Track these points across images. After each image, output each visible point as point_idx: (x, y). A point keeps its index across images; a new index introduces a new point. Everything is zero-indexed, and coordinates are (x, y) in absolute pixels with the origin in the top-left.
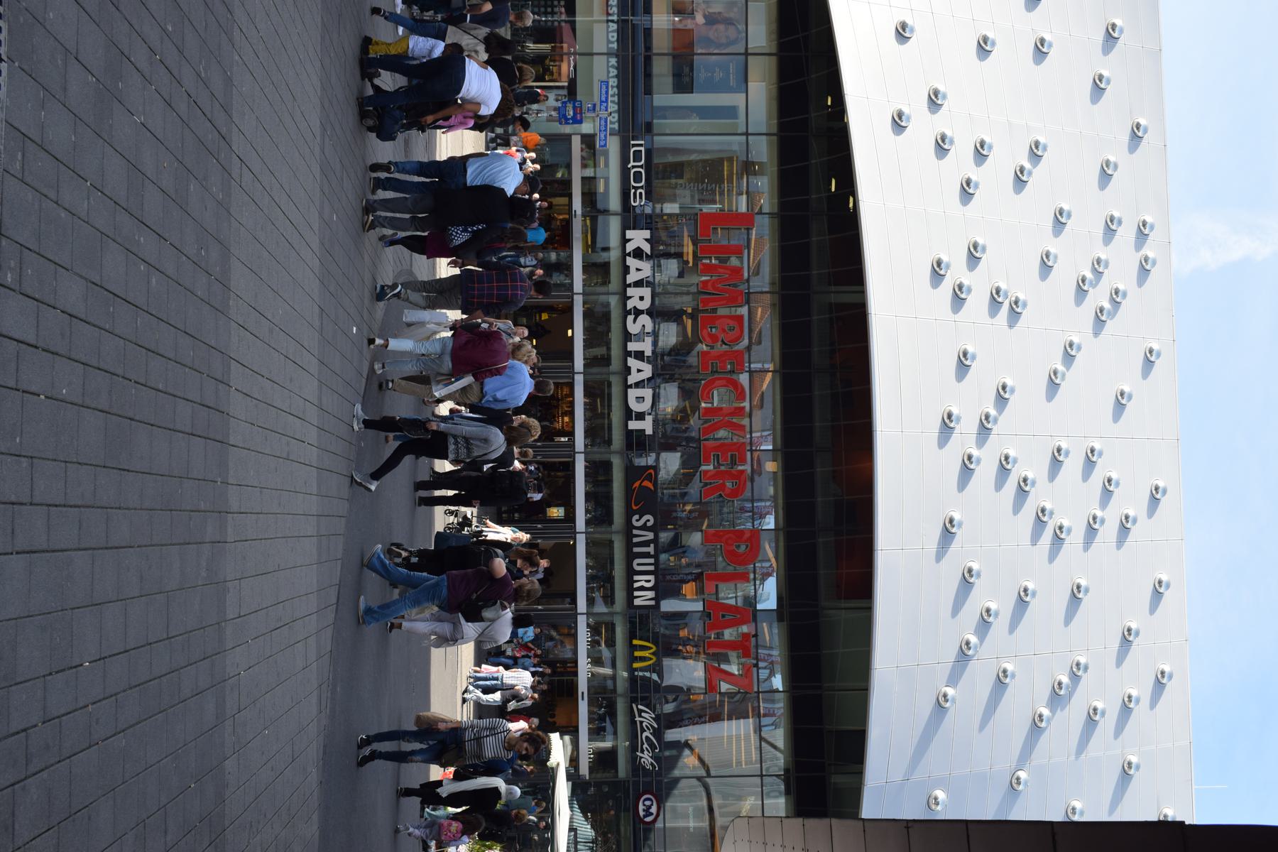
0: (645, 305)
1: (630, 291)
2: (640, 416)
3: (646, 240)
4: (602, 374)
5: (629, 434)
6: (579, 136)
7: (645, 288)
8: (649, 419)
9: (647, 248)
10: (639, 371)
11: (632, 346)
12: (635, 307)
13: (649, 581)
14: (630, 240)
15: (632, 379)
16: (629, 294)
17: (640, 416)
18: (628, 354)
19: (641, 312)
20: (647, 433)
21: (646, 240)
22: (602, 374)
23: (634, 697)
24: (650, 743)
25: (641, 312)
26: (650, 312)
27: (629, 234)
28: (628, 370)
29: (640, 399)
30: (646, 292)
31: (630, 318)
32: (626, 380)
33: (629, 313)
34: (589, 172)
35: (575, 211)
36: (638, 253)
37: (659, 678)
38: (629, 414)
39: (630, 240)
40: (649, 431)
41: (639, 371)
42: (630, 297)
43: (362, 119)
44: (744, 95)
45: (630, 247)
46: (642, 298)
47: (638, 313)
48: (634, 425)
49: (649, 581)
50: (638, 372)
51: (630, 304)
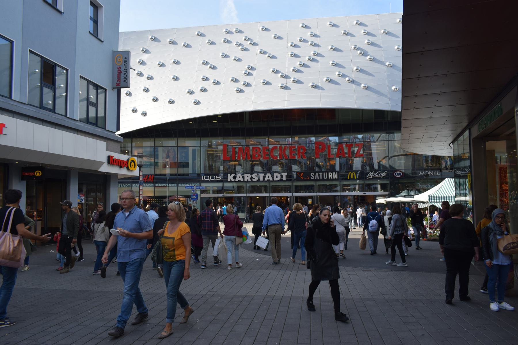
1: (246, 180)
2: (282, 177)
3: (231, 175)
5: (287, 180)
8: (283, 174)
9: (233, 175)
10: (269, 177)
11: (261, 179)
12: (250, 178)
14: (231, 180)
15: (271, 179)
16: (230, 181)
17: (282, 177)
18: (264, 180)
19: (252, 176)
20: (287, 175)
21: (231, 175)
25: (252, 176)
26: (252, 174)
27: (229, 180)
28: (268, 180)
29: (277, 177)
30: (246, 175)
31: (253, 180)
32: (242, 181)
34: (211, 192)
36: (235, 178)
38: (281, 180)
39: (231, 180)
40: (286, 174)
41: (269, 177)
42: (247, 180)
45: (233, 180)
46: (248, 176)
47: (252, 178)
48: (284, 179)
51: (249, 180)
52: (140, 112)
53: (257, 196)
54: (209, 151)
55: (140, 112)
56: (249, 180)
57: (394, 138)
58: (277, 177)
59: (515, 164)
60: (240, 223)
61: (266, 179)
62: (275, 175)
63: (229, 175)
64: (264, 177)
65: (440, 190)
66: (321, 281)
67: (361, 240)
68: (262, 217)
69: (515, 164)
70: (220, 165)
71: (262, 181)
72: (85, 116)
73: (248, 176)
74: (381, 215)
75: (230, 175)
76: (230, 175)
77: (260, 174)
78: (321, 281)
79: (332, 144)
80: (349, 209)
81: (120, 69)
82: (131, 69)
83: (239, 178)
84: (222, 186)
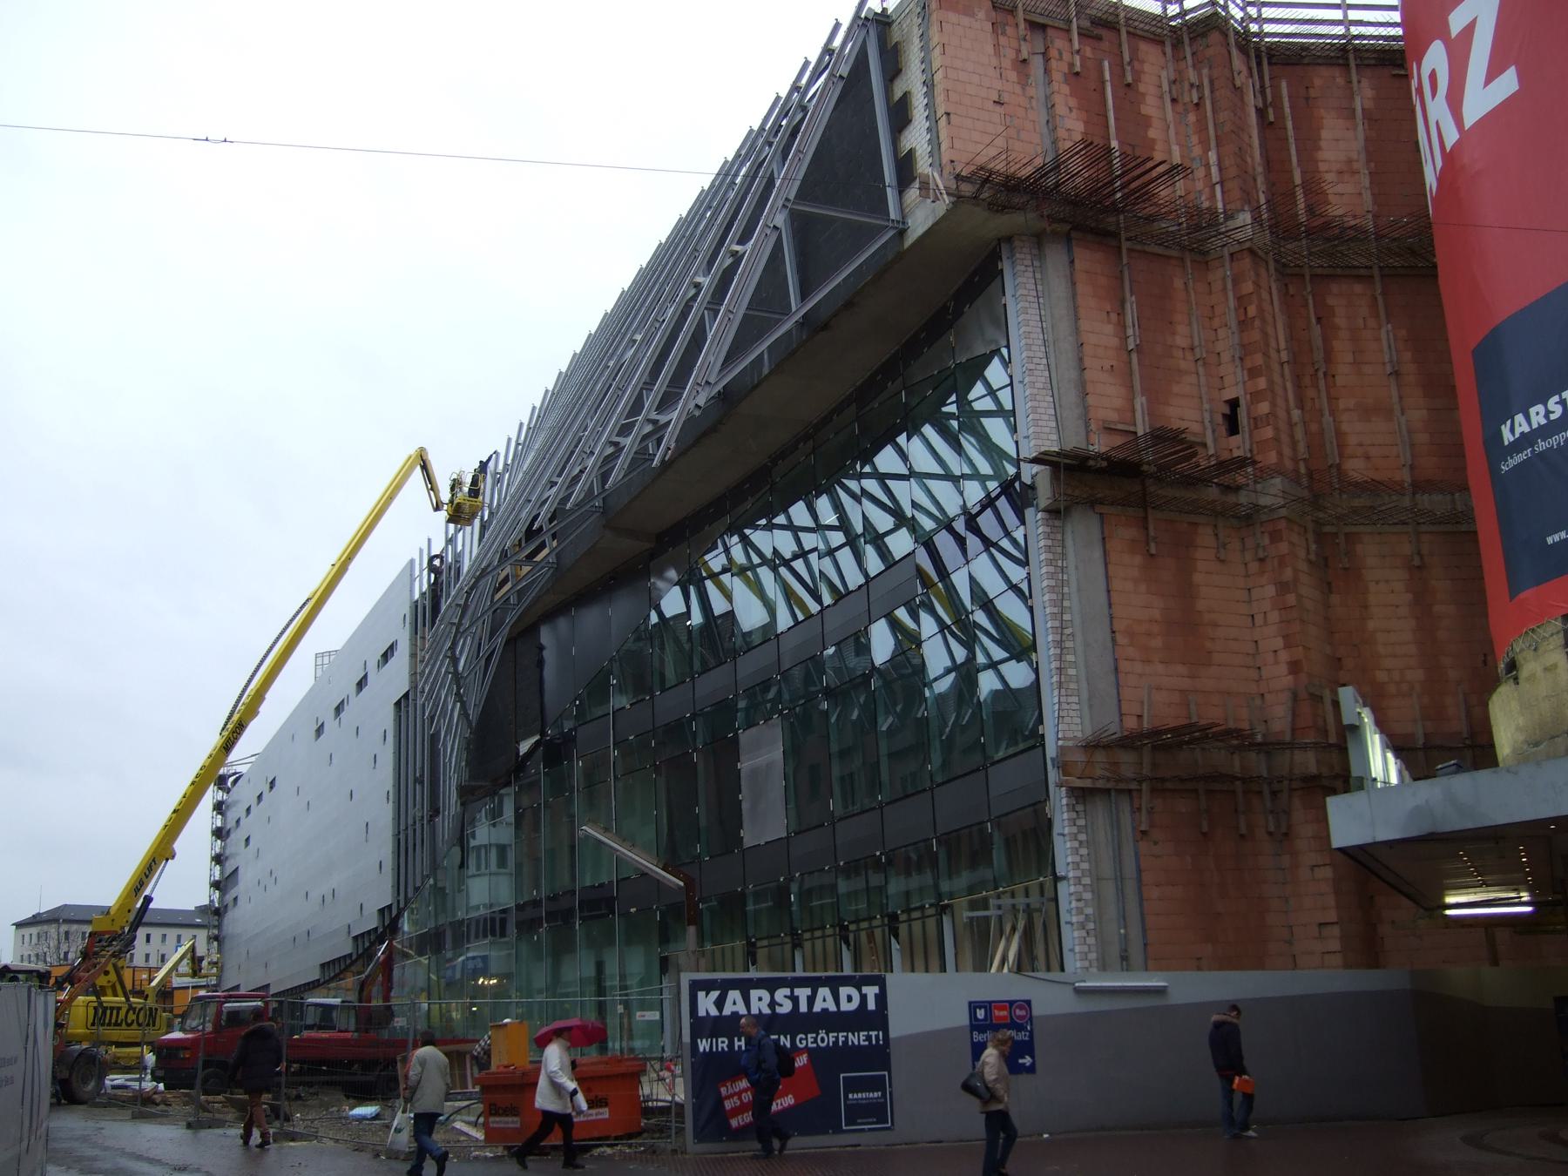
2: (864, 998)
11: (803, 1008)
29: (850, 999)
31: (779, 1010)
36: (720, 1003)
45: (714, 1012)
46: (760, 999)
51: (767, 1011)
53: (972, 1037)
54: (423, 787)
56: (767, 1011)
58: (850, 999)
60: (539, 1119)
61: (817, 1008)
64: (811, 1000)
65: (110, 1020)
68: (269, 1144)
70: (886, 971)
72: (949, 663)
73: (760, 999)
75: (704, 993)
76: (704, 993)
77: (797, 991)
79: (962, 832)
82: (1337, 923)
83: (735, 1003)
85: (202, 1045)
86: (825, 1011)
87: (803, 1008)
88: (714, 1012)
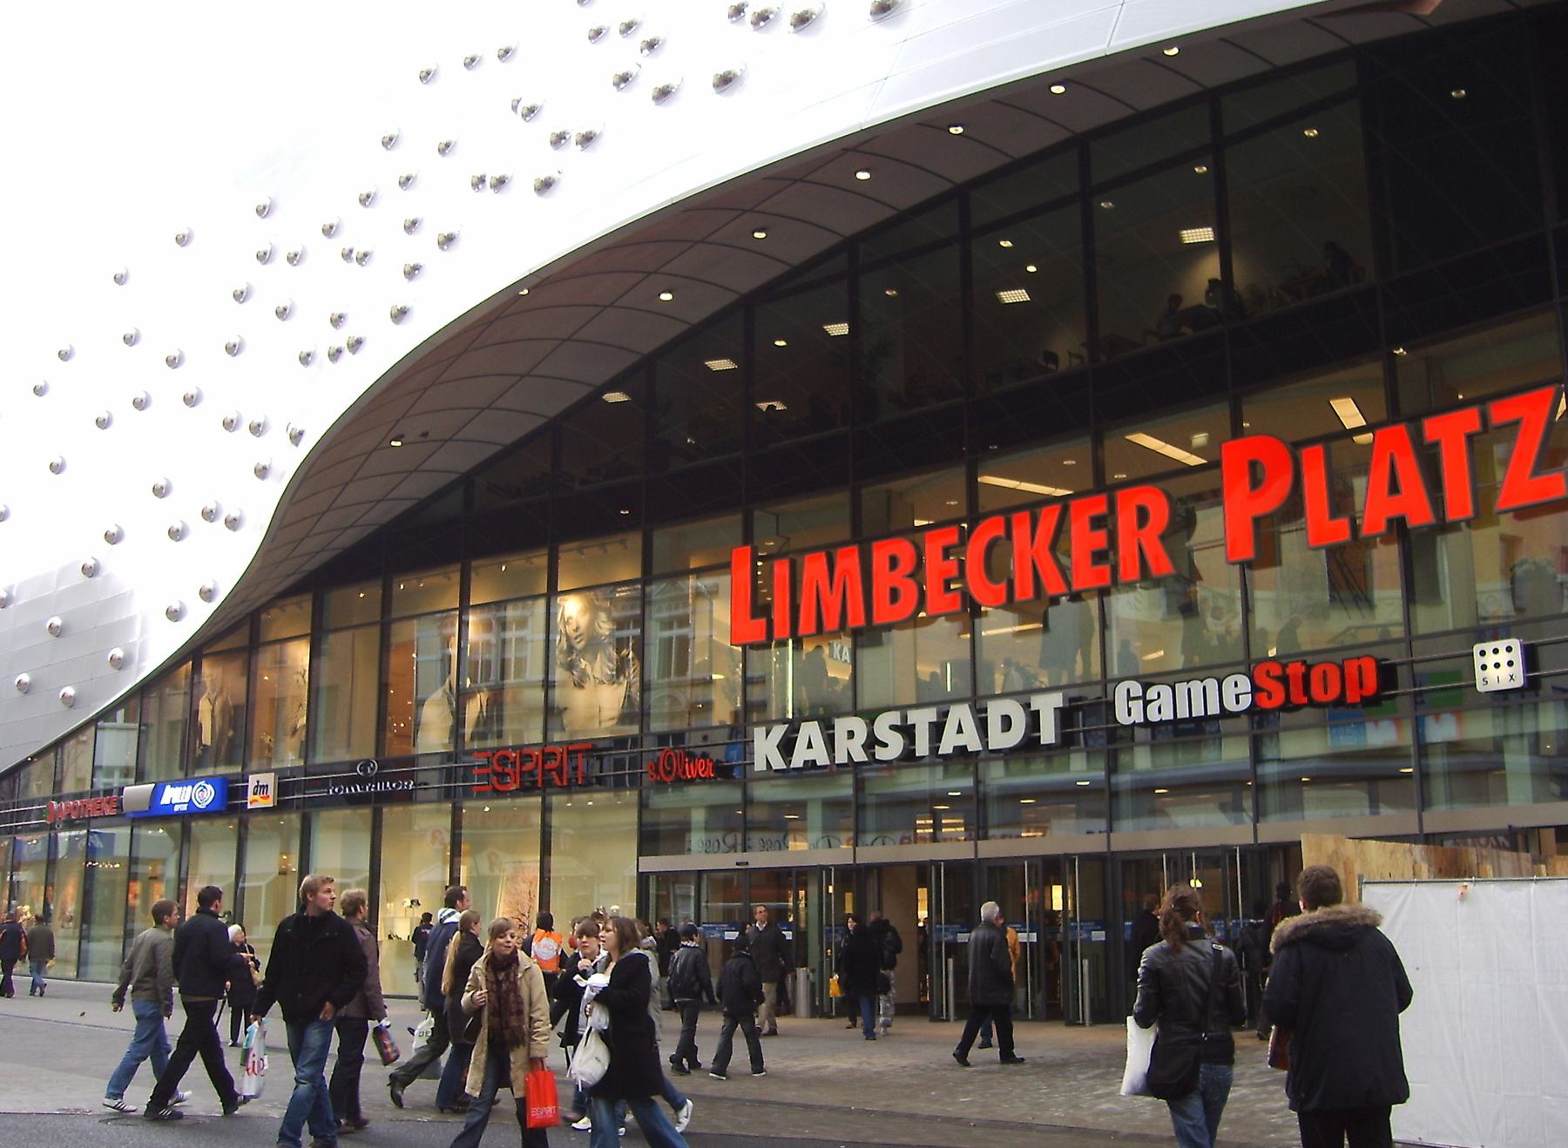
0: (858, 725)
1: (841, 758)
2: (1034, 719)
4: (1183, 865)
5: (1067, 741)
6: (1553, 830)
7: (948, 720)
11: (922, 748)
13: (1143, 515)
19: (871, 734)
22: (1183, 865)
23: (615, 780)
24: (243, 830)
25: (871, 734)
29: (1007, 723)
31: (881, 754)
33: (873, 759)
35: (737, 864)
36: (787, 747)
37: (182, 1041)
38: (1031, 743)
40: (1057, 700)
43: (387, 147)
44: (95, 764)
45: (778, 763)
47: (872, 742)
48: (1048, 735)
49: (1143, 515)
50: (812, 747)
51: (860, 756)
52: (124, 413)
55: (124, 413)
56: (860, 756)
57: (464, 770)
58: (1007, 723)
59: (949, 666)
62: (995, 710)
63: (759, 732)
64: (937, 730)
66: (1393, 1106)
67: (204, 697)
69: (949, 666)
71: (1049, 746)
73: (851, 734)
74: (916, 827)
78: (1393, 1106)
80: (569, 777)
81: (1493, 846)
84: (1258, 822)
85: (674, 640)
86: (811, 765)
87: (922, 747)
88: (778, 763)
